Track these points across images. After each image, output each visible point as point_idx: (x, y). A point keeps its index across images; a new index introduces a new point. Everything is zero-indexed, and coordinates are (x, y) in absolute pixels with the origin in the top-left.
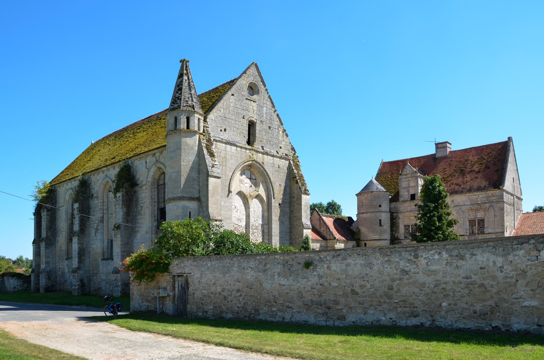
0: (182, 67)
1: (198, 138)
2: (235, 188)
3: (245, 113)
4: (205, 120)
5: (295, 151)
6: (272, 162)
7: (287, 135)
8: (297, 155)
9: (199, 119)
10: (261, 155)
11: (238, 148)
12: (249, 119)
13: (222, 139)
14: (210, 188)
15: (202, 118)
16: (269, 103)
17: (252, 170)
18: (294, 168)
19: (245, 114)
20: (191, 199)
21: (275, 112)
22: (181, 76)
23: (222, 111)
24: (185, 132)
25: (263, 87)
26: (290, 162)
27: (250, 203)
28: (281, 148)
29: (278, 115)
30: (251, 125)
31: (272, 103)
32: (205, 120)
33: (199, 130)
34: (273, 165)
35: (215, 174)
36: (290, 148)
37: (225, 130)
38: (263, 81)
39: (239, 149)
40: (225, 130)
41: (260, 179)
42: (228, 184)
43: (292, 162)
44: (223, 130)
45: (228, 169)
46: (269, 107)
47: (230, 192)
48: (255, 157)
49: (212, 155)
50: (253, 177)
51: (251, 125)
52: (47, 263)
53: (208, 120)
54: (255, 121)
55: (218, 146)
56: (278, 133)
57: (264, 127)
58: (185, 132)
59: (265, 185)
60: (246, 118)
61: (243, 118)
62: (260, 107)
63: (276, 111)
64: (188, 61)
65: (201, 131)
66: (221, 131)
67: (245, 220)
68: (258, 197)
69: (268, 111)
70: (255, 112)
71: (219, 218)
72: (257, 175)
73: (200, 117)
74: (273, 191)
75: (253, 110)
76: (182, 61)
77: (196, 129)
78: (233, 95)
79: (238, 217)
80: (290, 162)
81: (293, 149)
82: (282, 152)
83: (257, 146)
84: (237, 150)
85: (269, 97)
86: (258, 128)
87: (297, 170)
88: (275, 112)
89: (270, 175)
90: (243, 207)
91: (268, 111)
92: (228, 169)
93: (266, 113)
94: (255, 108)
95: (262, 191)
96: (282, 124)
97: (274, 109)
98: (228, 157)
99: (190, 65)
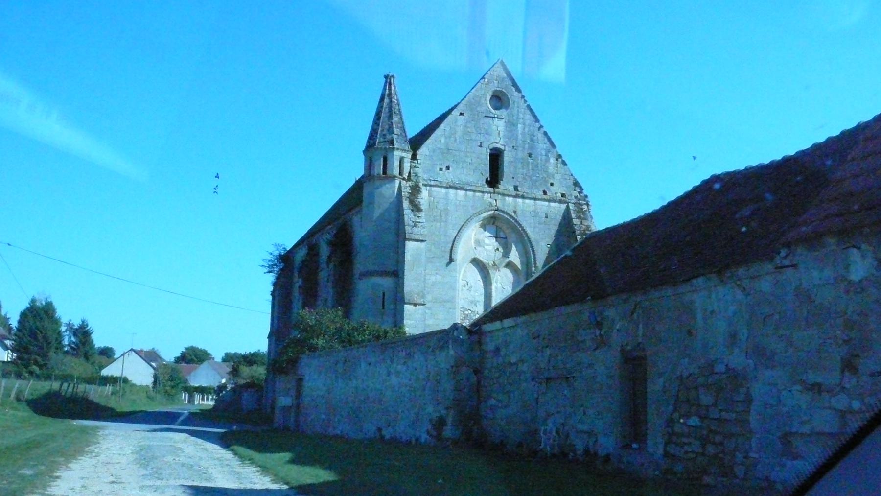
0: (386, 82)
1: (397, 185)
2: (462, 253)
3: (482, 138)
4: (414, 157)
5: (580, 187)
6: (532, 208)
7: (564, 163)
8: (585, 192)
9: (401, 160)
10: (511, 199)
11: (469, 193)
12: (491, 147)
13: (441, 182)
14: (408, 257)
15: (408, 156)
16: (528, 116)
17: (498, 223)
18: (573, 216)
19: (482, 140)
20: (384, 273)
21: (539, 129)
22: (382, 99)
23: (443, 141)
24: (380, 178)
25: (516, 94)
26: (568, 207)
27: (492, 275)
28: (552, 184)
29: (545, 133)
30: (496, 157)
31: (535, 116)
32: (414, 157)
33: (401, 173)
34: (535, 214)
35: (417, 237)
36: (571, 183)
37: (448, 168)
38: (515, 85)
39: (470, 194)
40: (448, 168)
41: (512, 237)
42: (449, 249)
43: (571, 207)
44: (444, 169)
45: (451, 226)
46: (528, 122)
47: (451, 260)
48: (500, 204)
49: (416, 208)
50: (502, 235)
51: (496, 157)
52: (491, 332)
53: (418, 157)
54: (502, 148)
55: (434, 194)
56: (547, 160)
57: (520, 155)
58: (380, 178)
59: (520, 246)
60: (485, 145)
61: (481, 146)
62: (511, 125)
63: (541, 127)
64: (393, 76)
65: (406, 176)
66: (441, 169)
67: (482, 304)
68: (509, 265)
69: (527, 130)
70: (501, 135)
71: (421, 301)
72: (507, 231)
73: (404, 154)
74: (534, 255)
75: (497, 132)
76: (386, 77)
77: (396, 172)
78: (461, 114)
79: (471, 299)
80: (568, 207)
81: (576, 184)
82: (557, 190)
83: (506, 185)
84: (466, 195)
85: (529, 107)
86: (507, 158)
87: (579, 218)
88: (539, 129)
89: (529, 231)
90: (481, 283)
91: (527, 130)
92: (451, 226)
93: (523, 134)
94: (501, 128)
95: (515, 257)
96: (554, 146)
97: (538, 125)
98: (451, 208)
99: (396, 81)
